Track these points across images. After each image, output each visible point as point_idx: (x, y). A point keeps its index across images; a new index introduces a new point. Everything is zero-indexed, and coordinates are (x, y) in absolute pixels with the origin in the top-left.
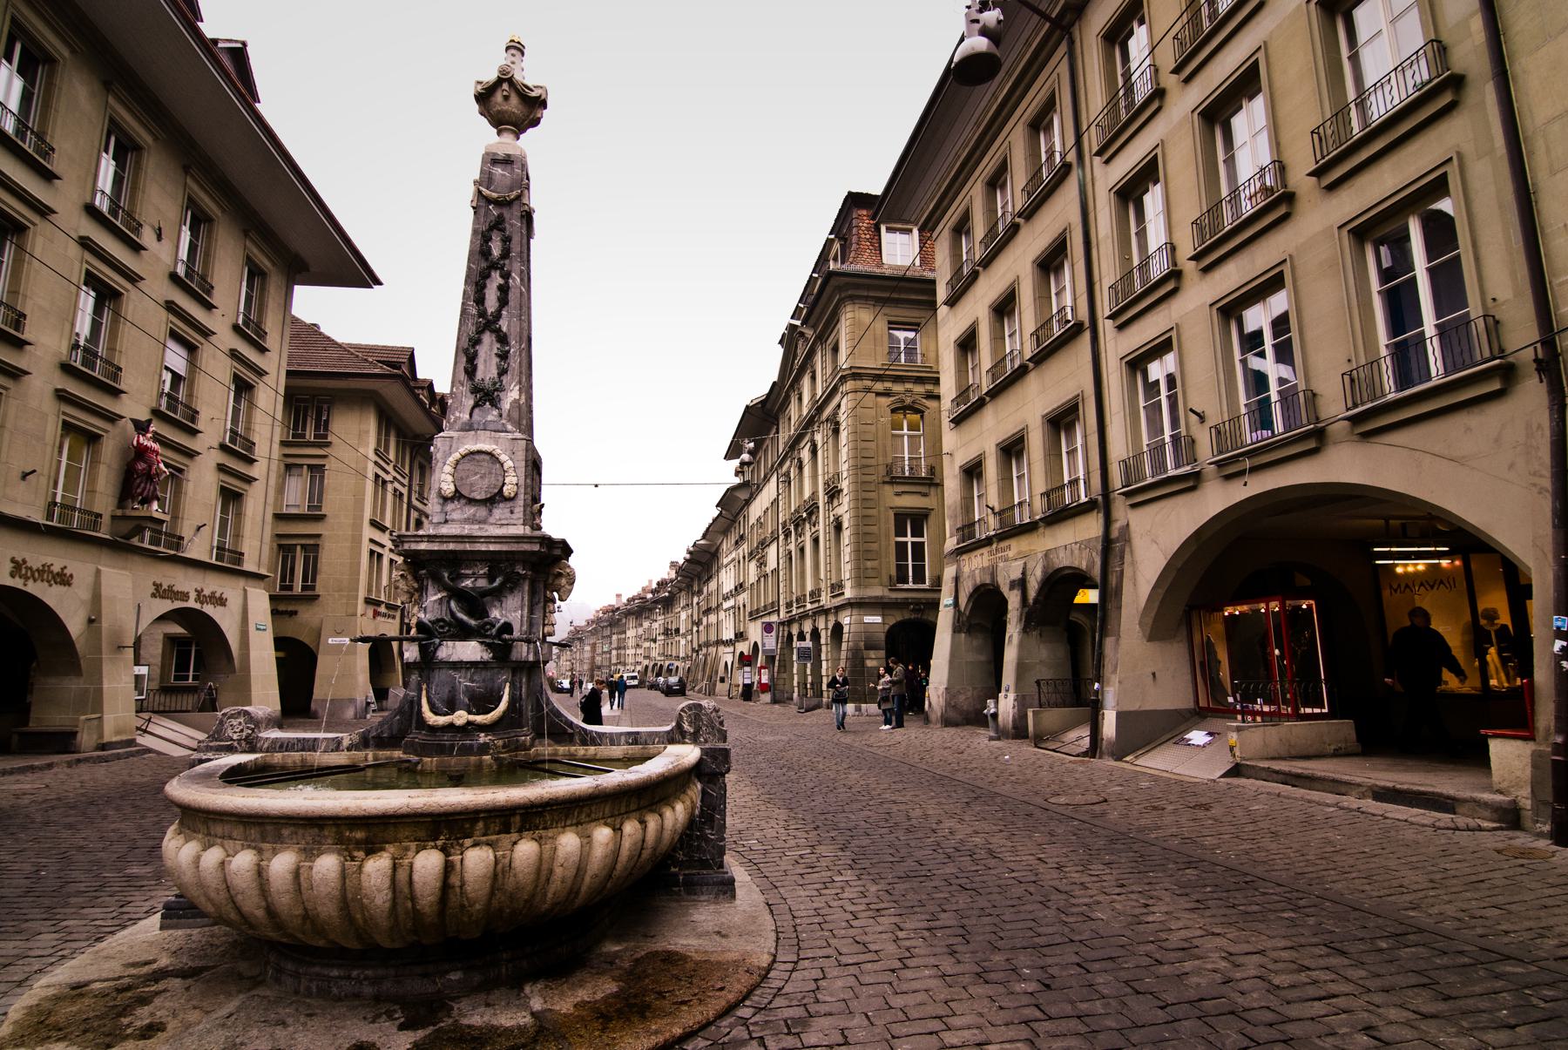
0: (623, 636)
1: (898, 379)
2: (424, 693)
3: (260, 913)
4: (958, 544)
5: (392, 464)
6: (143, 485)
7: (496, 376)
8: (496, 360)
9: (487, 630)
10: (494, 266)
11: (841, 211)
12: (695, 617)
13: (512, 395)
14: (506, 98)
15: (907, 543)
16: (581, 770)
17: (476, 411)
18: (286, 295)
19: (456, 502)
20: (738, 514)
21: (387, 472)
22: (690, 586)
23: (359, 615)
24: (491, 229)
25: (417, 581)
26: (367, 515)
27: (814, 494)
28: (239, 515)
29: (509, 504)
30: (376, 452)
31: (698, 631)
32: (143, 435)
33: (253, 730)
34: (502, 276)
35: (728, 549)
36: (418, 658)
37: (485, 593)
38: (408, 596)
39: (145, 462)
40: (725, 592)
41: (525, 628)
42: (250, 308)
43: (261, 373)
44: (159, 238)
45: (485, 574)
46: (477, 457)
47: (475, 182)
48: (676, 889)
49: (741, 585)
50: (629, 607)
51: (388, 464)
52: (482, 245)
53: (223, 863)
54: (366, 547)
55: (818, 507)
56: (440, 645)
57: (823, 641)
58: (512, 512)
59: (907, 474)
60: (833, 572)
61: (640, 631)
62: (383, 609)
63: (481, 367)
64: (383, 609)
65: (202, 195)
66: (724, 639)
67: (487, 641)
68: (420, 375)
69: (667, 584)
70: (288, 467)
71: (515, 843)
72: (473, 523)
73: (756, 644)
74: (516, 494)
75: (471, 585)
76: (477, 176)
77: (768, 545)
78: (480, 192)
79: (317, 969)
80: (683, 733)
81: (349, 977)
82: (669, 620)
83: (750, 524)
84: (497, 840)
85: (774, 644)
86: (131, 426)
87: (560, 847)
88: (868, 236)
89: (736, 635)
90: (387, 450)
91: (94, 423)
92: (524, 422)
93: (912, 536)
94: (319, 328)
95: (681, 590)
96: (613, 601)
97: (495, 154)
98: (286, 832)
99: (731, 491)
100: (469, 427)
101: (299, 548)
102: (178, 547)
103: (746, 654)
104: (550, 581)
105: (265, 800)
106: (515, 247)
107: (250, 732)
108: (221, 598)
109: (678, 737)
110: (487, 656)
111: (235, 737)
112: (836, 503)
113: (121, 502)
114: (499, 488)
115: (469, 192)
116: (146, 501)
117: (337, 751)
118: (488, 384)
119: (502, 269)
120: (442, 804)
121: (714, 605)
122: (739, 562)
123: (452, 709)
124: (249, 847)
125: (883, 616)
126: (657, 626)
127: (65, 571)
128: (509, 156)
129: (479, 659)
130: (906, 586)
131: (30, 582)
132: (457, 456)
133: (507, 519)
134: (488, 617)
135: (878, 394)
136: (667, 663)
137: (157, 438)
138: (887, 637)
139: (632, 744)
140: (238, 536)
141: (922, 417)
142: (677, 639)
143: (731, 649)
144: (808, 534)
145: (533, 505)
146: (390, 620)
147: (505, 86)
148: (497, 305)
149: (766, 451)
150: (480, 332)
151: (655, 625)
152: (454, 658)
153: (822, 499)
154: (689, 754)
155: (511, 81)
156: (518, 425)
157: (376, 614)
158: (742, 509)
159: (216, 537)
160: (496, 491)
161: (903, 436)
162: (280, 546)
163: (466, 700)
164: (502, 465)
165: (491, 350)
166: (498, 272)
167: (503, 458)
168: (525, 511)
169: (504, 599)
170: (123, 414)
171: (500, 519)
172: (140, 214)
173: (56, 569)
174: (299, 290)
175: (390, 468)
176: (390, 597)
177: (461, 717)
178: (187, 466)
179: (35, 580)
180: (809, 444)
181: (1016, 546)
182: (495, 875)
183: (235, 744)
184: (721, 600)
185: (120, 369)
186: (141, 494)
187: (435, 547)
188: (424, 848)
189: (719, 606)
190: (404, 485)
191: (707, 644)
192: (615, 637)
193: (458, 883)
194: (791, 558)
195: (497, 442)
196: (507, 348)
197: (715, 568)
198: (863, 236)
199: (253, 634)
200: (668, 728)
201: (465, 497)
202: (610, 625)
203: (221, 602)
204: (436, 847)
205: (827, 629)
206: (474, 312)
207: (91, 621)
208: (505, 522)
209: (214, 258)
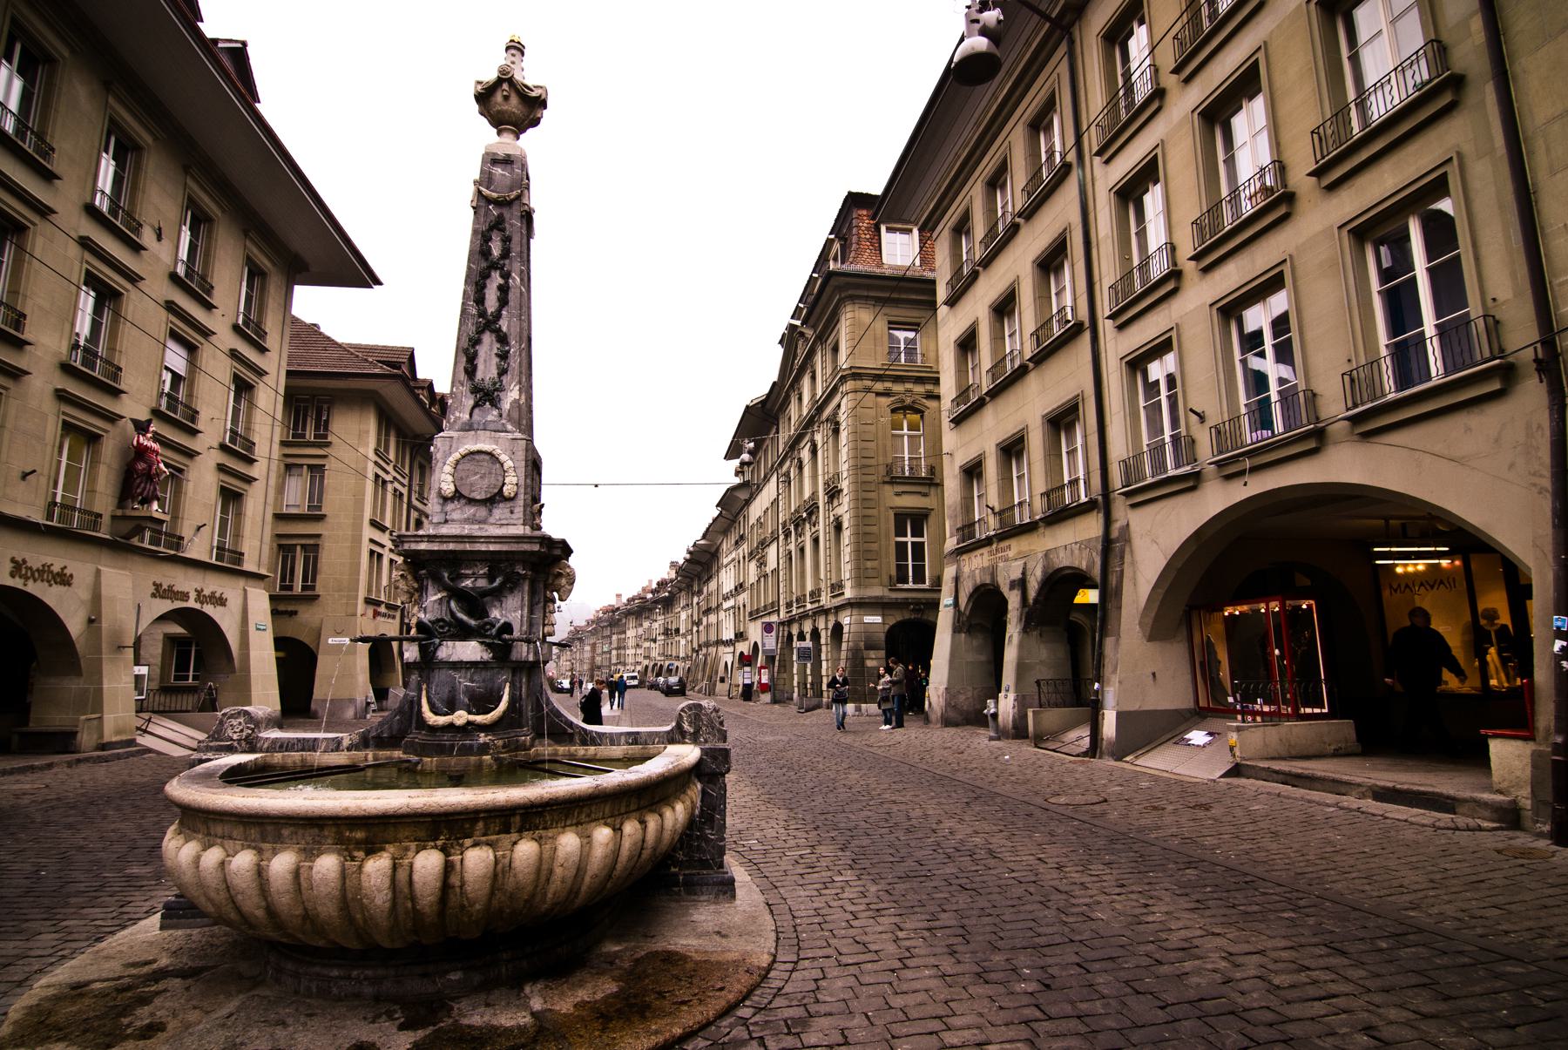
0: (623, 636)
1: (898, 379)
2: (424, 693)
3: (260, 913)
4: (958, 544)
6: (143, 485)
7: (496, 376)
8: (495, 360)
9: (487, 630)
10: (494, 266)
11: (841, 211)
12: (695, 618)
13: (512, 395)
14: (506, 98)
15: (907, 543)
16: (581, 770)
17: (476, 411)
18: (286, 295)
19: (456, 502)
20: (739, 513)
21: (387, 473)
22: (690, 586)
23: (359, 615)
24: (491, 228)
26: (367, 515)
27: (814, 494)
28: (239, 515)
29: (509, 504)
30: (376, 452)
31: (698, 631)
32: (144, 435)
33: (253, 730)
34: (502, 276)
37: (485, 593)
38: (408, 595)
40: (724, 592)
41: (524, 628)
44: (159, 238)
45: (485, 574)
46: (477, 457)
48: (676, 889)
49: (741, 585)
50: (629, 607)
51: (388, 464)
52: (481, 245)
54: (366, 547)
55: (818, 507)
56: (440, 645)
57: (823, 641)
58: (512, 512)
59: (907, 474)
60: (833, 571)
61: (640, 631)
62: (382, 609)
63: (481, 367)
64: (382, 609)
66: (724, 639)
67: (487, 641)
68: (420, 375)
69: (667, 584)
70: (288, 467)
71: (515, 843)
72: (473, 523)
73: (756, 643)
74: (516, 494)
75: (471, 585)
76: (477, 176)
77: (768, 545)
78: (479, 192)
81: (349, 978)
82: (669, 620)
83: (750, 524)
84: (497, 840)
85: (774, 644)
86: (131, 426)
87: (560, 848)
88: (868, 236)
89: (736, 635)
90: (387, 450)
92: (524, 422)
93: (912, 536)
94: (319, 328)
95: (681, 590)
97: (494, 154)
98: (286, 832)
99: (732, 491)
100: (469, 427)
101: (299, 548)
103: (746, 654)
104: (550, 581)
106: (515, 248)
107: (250, 732)
108: (221, 598)
109: (678, 737)
110: (487, 656)
111: (235, 737)
112: (836, 503)
115: (469, 192)
116: (146, 501)
117: (337, 751)
118: (488, 384)
119: (502, 269)
120: (442, 804)
121: (714, 605)
124: (249, 847)
125: (883, 616)
126: (657, 626)
127: (65, 571)
128: (508, 155)
129: (479, 659)
130: (906, 586)
131: (30, 582)
132: (457, 456)
133: (506, 519)
134: (488, 617)
136: (667, 663)
137: (157, 438)
139: (632, 744)
140: (238, 535)
141: (922, 417)
142: (677, 639)
143: (731, 649)
144: (808, 534)
145: (533, 505)
146: (390, 620)
147: (505, 86)
148: (497, 304)
149: (766, 451)
151: (656, 625)
152: (454, 658)
153: (822, 499)
154: (689, 754)
155: (511, 81)
156: (518, 425)
157: (376, 614)
158: (742, 509)
159: (216, 537)
160: (496, 491)
161: (903, 436)
162: (280, 546)
163: (466, 700)
164: (502, 465)
165: (491, 350)
166: (498, 272)
167: (503, 458)
168: (525, 511)
169: (504, 599)
171: (500, 519)
173: (56, 569)
174: (299, 290)
175: (390, 468)
177: (461, 717)
179: (35, 580)
180: (809, 444)
181: (1016, 546)
182: (495, 875)
183: (235, 744)
184: (721, 600)
186: (141, 494)
187: (435, 547)
188: (424, 848)
189: (719, 606)
190: (404, 485)
192: (614, 637)
193: (458, 883)
194: (791, 559)
195: (496, 442)
196: (507, 348)
197: (715, 569)
198: (863, 236)
199: (253, 635)
200: (668, 728)
201: (465, 497)
202: (610, 625)
203: (221, 602)
204: (436, 847)
205: (827, 629)
206: (474, 312)
208: (503, 522)
209: (214, 257)
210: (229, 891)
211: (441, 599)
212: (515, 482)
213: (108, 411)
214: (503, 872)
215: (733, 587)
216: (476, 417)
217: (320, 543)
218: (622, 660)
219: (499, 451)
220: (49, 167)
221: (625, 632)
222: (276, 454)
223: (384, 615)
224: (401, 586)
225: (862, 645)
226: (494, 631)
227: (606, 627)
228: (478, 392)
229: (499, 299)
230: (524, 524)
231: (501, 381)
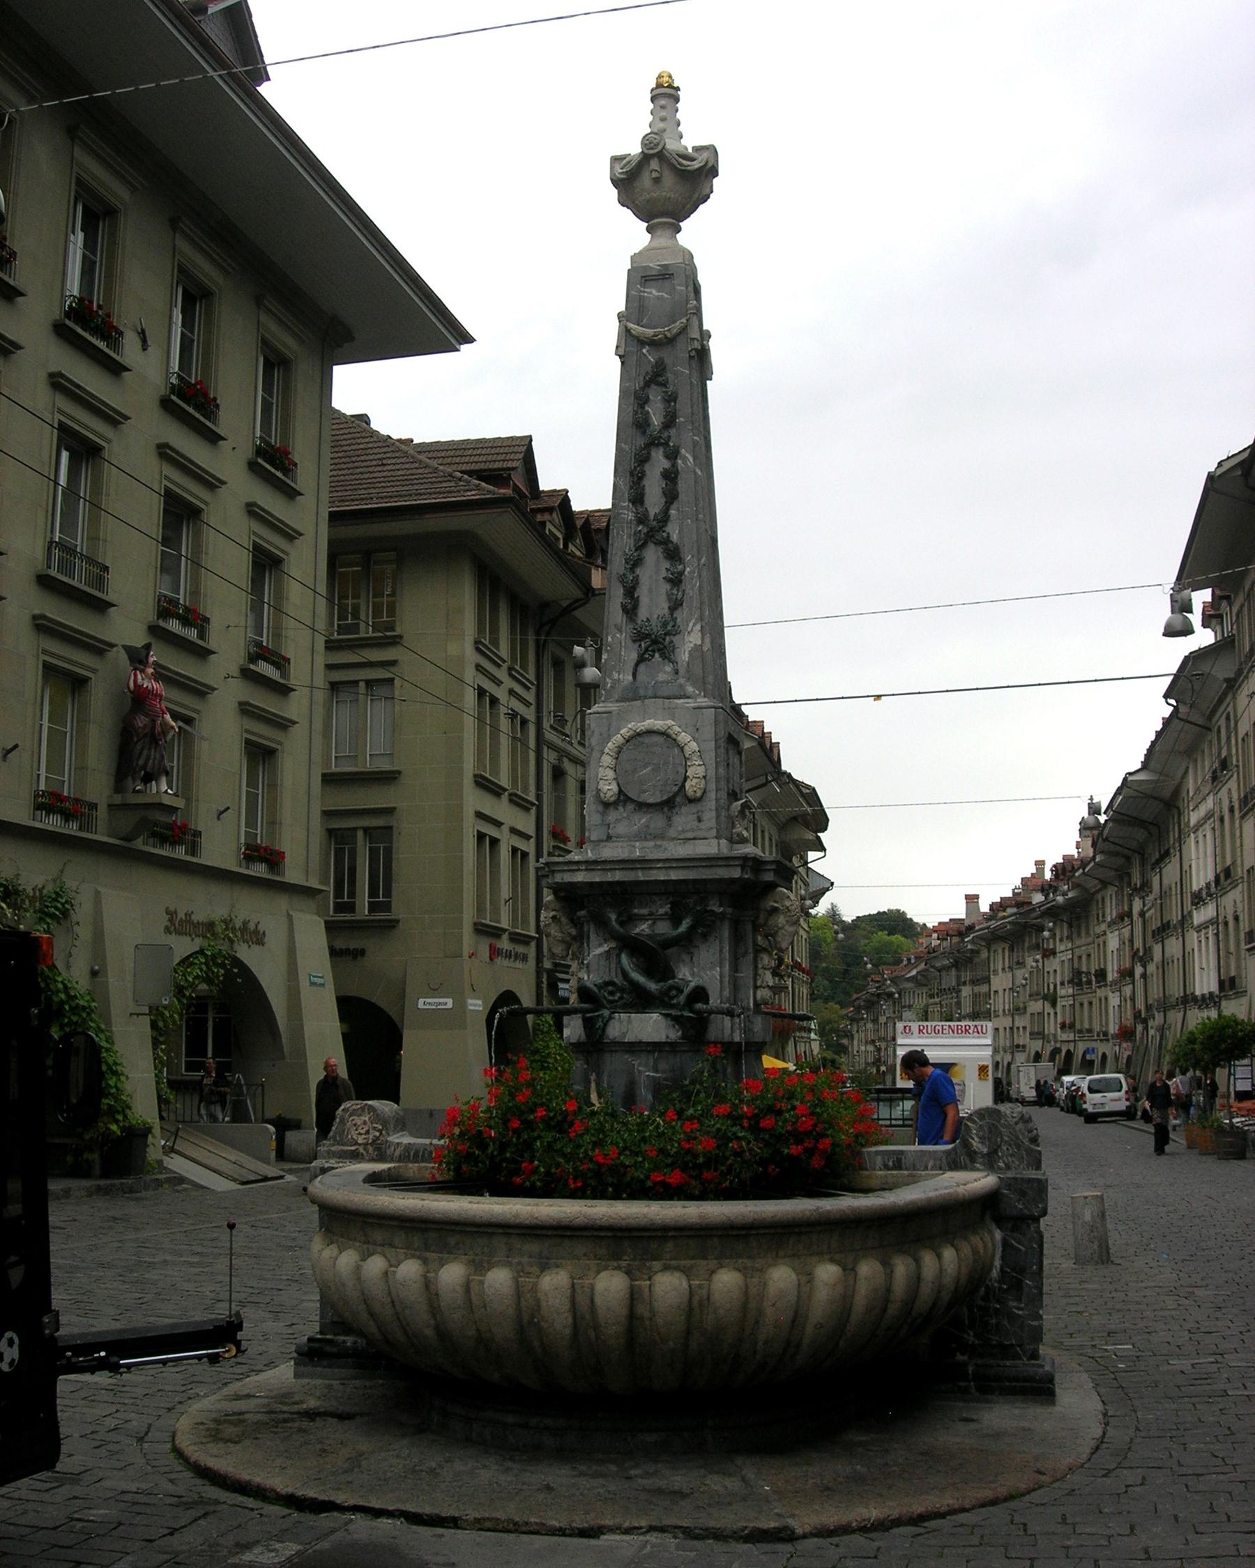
0: (983, 989)
2: (593, 1085)
3: (429, 1332)
5: (505, 666)
6: (145, 752)
7: (666, 611)
8: (665, 587)
9: (672, 998)
10: (653, 443)
12: (1138, 944)
13: (690, 639)
14: (657, 181)
17: (642, 668)
18: (321, 396)
19: (621, 809)
20: (1214, 712)
21: (498, 683)
22: (1123, 875)
23: (466, 953)
24: (647, 384)
25: (575, 926)
26: (469, 768)
28: (273, 786)
29: (693, 808)
30: (478, 647)
31: (1144, 976)
32: (142, 671)
33: (380, 1131)
34: (667, 457)
35: (1197, 790)
36: (583, 1037)
37: (667, 943)
39: (146, 715)
40: (1195, 888)
41: (726, 993)
42: (270, 423)
43: (291, 535)
44: (145, 346)
45: (666, 914)
46: (647, 740)
47: (620, 316)
48: (962, 1384)
49: (1227, 872)
50: (993, 924)
51: (499, 666)
52: (636, 412)
53: (386, 1273)
54: (470, 827)
56: (611, 1018)
58: (699, 820)
61: (1020, 973)
62: (504, 944)
63: (644, 601)
64: (504, 944)
65: (200, 260)
67: (673, 1012)
68: (545, 484)
69: (1074, 870)
70: (334, 687)
71: (713, 1272)
72: (646, 839)
74: (704, 792)
75: (648, 931)
78: (628, 331)
80: (972, 1155)
82: (1082, 951)
84: (692, 1267)
86: (123, 657)
87: (771, 1283)
89: (1221, 984)
90: (495, 641)
91: (80, 660)
92: (710, 679)
94: (368, 422)
95: (1105, 884)
98: (452, 1240)
100: (633, 695)
101: (360, 834)
102: (193, 850)
104: (761, 920)
105: (427, 1202)
106: (684, 407)
107: (378, 1134)
108: (256, 932)
109: (964, 1159)
110: (674, 1034)
113: (119, 787)
115: (610, 332)
116: (148, 778)
118: (656, 627)
119: (666, 444)
120: (623, 1216)
121: (1174, 916)
122: (1222, 819)
124: (413, 1256)
129: (663, 1039)
132: (618, 739)
134: (674, 977)
136: (1081, 1047)
137: (162, 674)
139: (893, 1169)
140: (273, 823)
142: (1101, 993)
145: (731, 803)
146: (519, 964)
147: (654, 164)
148: (663, 500)
150: (640, 548)
151: (1053, 964)
155: (662, 156)
156: (702, 684)
157: (494, 953)
158: (1220, 701)
160: (675, 789)
162: (330, 832)
163: (650, 1097)
164: (682, 749)
165: (657, 572)
167: (684, 737)
168: (718, 817)
170: (113, 641)
171: (683, 831)
172: (120, 316)
175: (502, 674)
176: (515, 919)
178: (197, 711)
182: (690, 1309)
183: (361, 1150)
185: (106, 569)
186: (144, 767)
187: (597, 877)
188: (606, 1268)
189: (1185, 919)
191: (1165, 1006)
192: (966, 991)
193: (647, 1314)
196: (680, 567)
201: (633, 801)
202: (956, 965)
204: (618, 1268)
206: (631, 516)
207: (94, 974)
208: (689, 835)
210: (394, 1306)
211: (608, 952)
212: (701, 775)
213: (88, 636)
214: (701, 1304)
215: (1211, 876)
216: (640, 677)
217: (394, 824)
219: (677, 729)
220: (11, 282)
221: (987, 980)
222: (320, 680)
223: (508, 955)
224: (553, 932)
226: (682, 999)
227: (947, 968)
228: (643, 639)
230: (718, 837)
231: (674, 620)
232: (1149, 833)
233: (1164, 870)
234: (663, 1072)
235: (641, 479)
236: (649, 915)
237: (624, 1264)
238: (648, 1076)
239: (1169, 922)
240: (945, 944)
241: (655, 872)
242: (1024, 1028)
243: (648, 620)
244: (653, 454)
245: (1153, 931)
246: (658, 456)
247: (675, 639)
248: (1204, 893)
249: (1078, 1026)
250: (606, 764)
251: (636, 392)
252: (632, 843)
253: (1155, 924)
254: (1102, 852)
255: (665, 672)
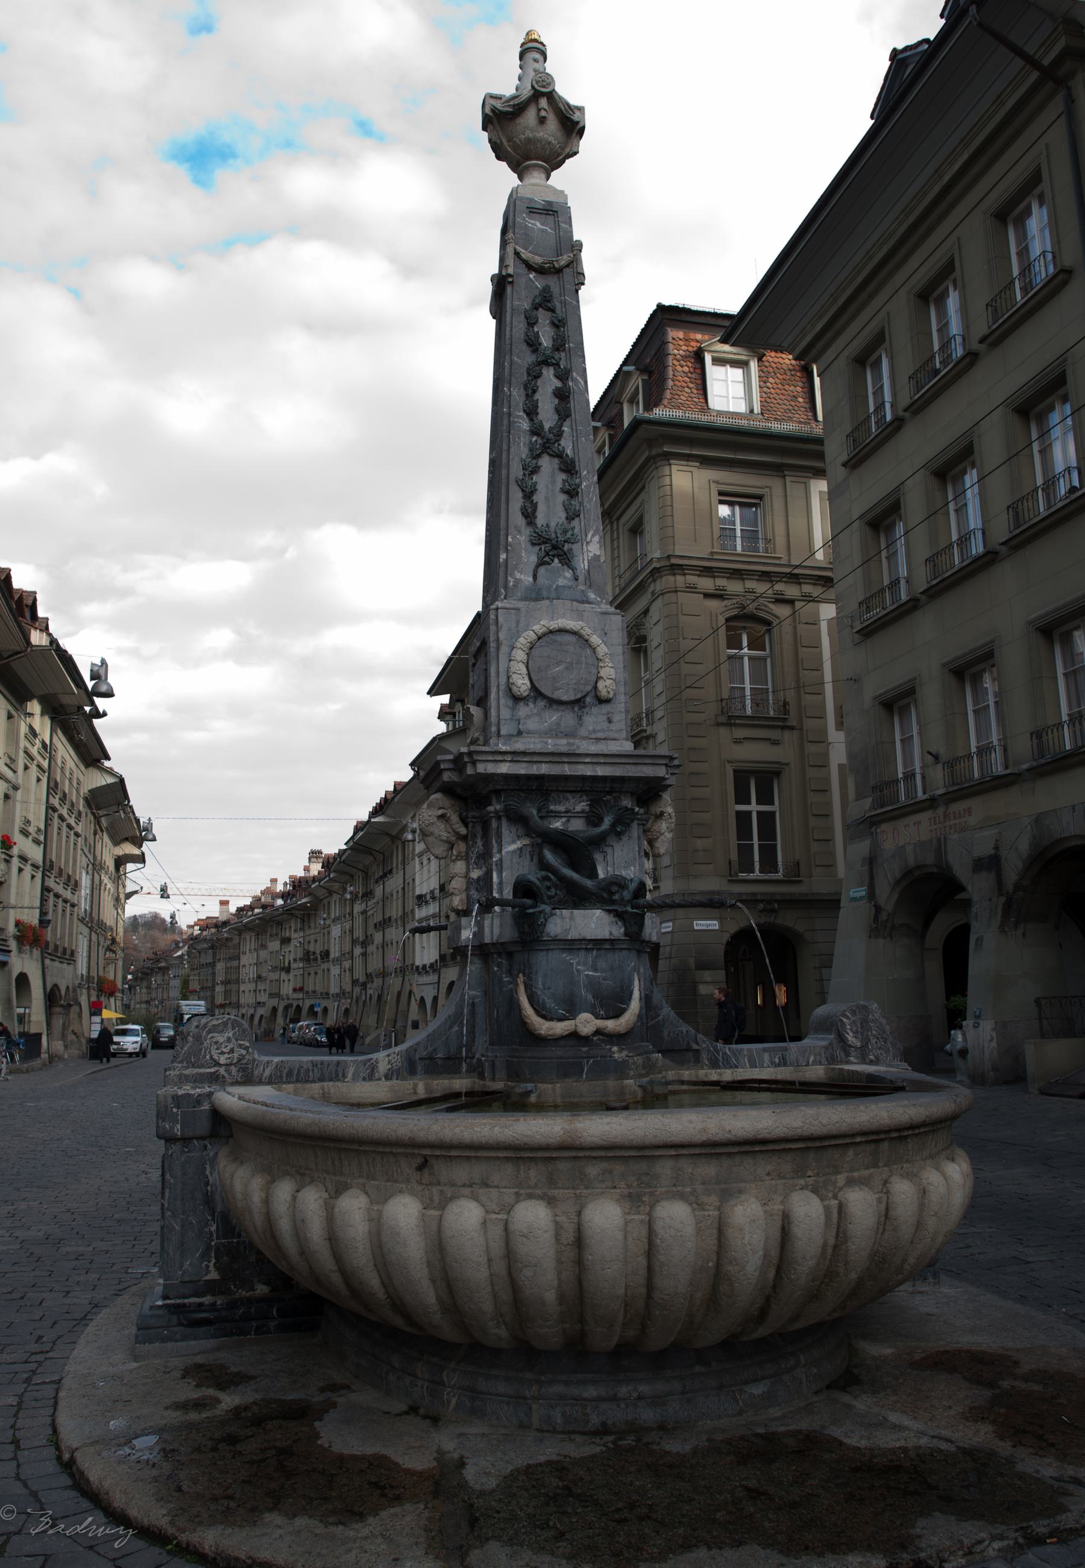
0: (235, 963)
1: (737, 574)
4: (873, 808)
11: (643, 331)
12: (359, 933)
14: (542, 121)
15: (749, 813)
19: (531, 705)
24: (536, 307)
29: (605, 708)
34: (557, 377)
38: (447, 846)
45: (583, 812)
46: (559, 638)
56: (552, 915)
58: (610, 721)
59: (749, 712)
61: (264, 954)
66: (418, 962)
79: (558, 1389)
81: (614, 1399)
82: (312, 938)
88: (686, 369)
93: (758, 803)
96: (213, 910)
97: (531, 200)
98: (593, 1170)
100: (535, 595)
111: (223, 1060)
114: (592, 683)
123: (571, 1013)
125: (721, 920)
126: (293, 951)
128: (550, 203)
130: (752, 876)
133: (603, 731)
135: (707, 596)
136: (308, 1003)
138: (726, 953)
139: (779, 1065)
141: (769, 631)
142: (324, 966)
143: (433, 978)
147: (543, 102)
152: (573, 935)
160: (589, 688)
161: (741, 658)
163: (590, 997)
166: (551, 370)
167: (595, 639)
169: (609, 850)
171: (594, 731)
177: (586, 1023)
181: (977, 809)
183: (222, 1071)
184: (411, 903)
187: (521, 769)
192: (220, 966)
195: (580, 616)
198: (679, 368)
202: (213, 947)
208: (600, 735)
211: (521, 849)
216: (542, 580)
218: (234, 999)
225: (692, 962)
226: (627, 895)
229: (557, 410)
232: (375, 858)
233: (387, 883)
234: (603, 971)
235: (534, 391)
236: (566, 812)
237: (811, 1181)
238: (587, 975)
239: (390, 918)
240: (205, 933)
241: (582, 767)
242: (265, 990)
243: (548, 526)
244: (544, 372)
245: (375, 924)
246: (548, 373)
247: (574, 547)
248: (428, 896)
249: (306, 989)
250: (519, 659)
251: (526, 311)
252: (545, 740)
253: (379, 918)
254: (334, 871)
255: (565, 578)
